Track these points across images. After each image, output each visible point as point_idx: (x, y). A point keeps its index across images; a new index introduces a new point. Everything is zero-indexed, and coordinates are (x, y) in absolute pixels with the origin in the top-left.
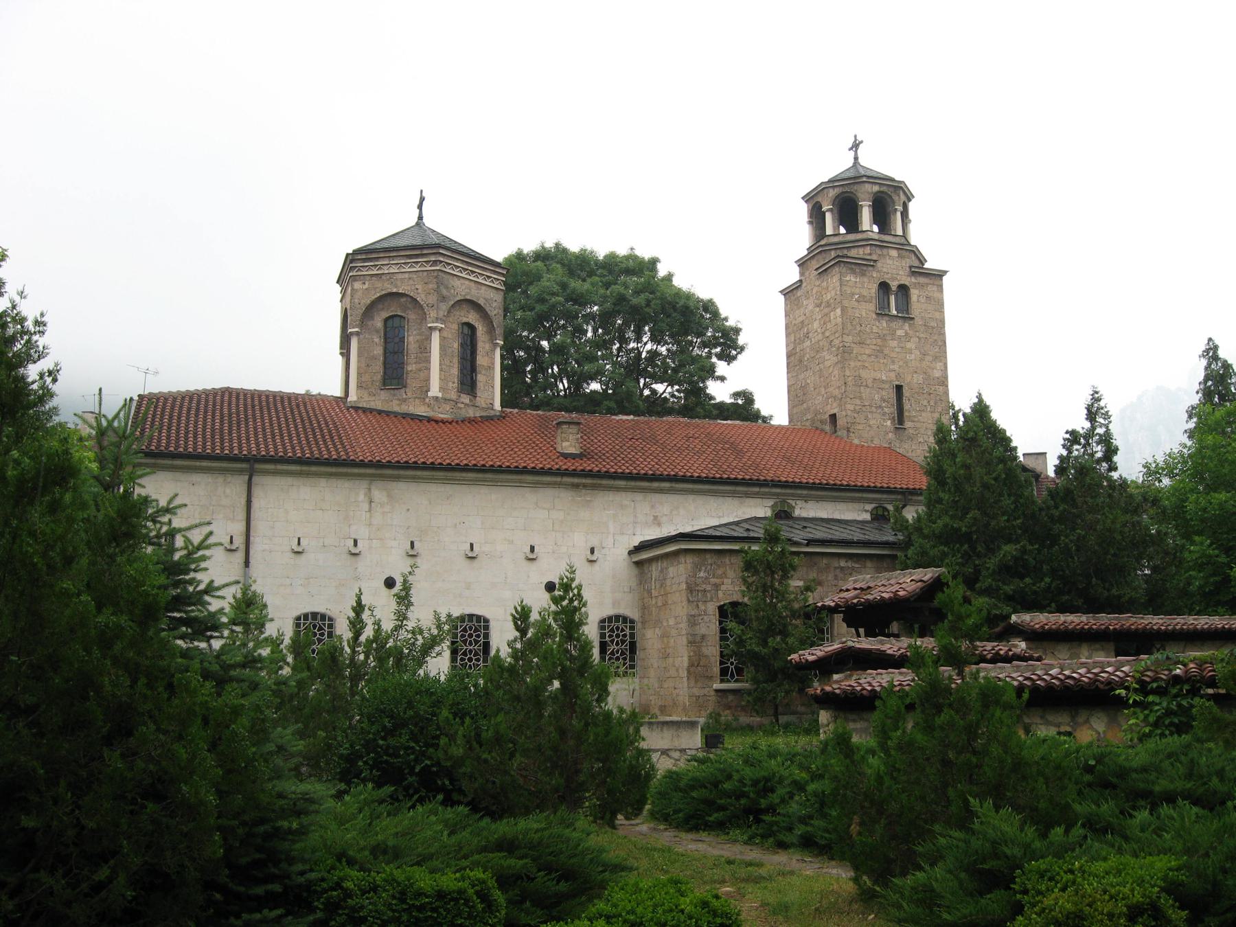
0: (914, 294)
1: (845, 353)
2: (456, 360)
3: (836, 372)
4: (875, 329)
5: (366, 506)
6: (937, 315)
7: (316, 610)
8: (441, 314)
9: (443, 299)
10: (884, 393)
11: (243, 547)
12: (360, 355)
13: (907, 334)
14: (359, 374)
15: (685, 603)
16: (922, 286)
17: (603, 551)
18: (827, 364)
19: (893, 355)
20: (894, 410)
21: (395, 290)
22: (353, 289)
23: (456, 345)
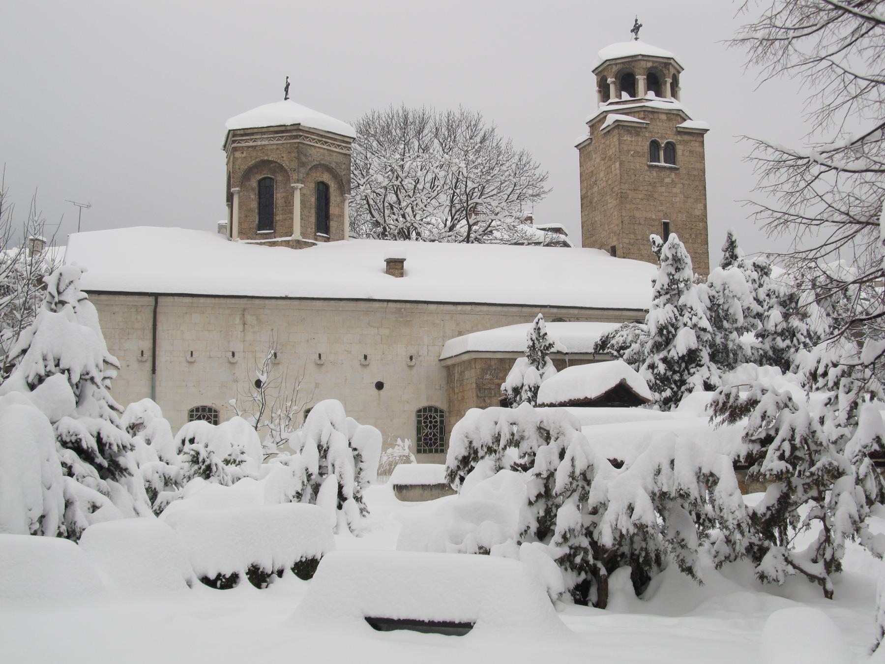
0: (679, 149)
1: (622, 198)
2: (313, 211)
3: (616, 213)
4: (647, 179)
5: (241, 327)
6: (699, 165)
7: (205, 404)
8: (301, 175)
9: (303, 165)
11: (151, 359)
12: (240, 208)
13: (673, 181)
14: (240, 223)
15: (475, 398)
17: (420, 359)
18: (610, 206)
19: (662, 198)
21: (266, 158)
22: (234, 158)
23: (313, 200)
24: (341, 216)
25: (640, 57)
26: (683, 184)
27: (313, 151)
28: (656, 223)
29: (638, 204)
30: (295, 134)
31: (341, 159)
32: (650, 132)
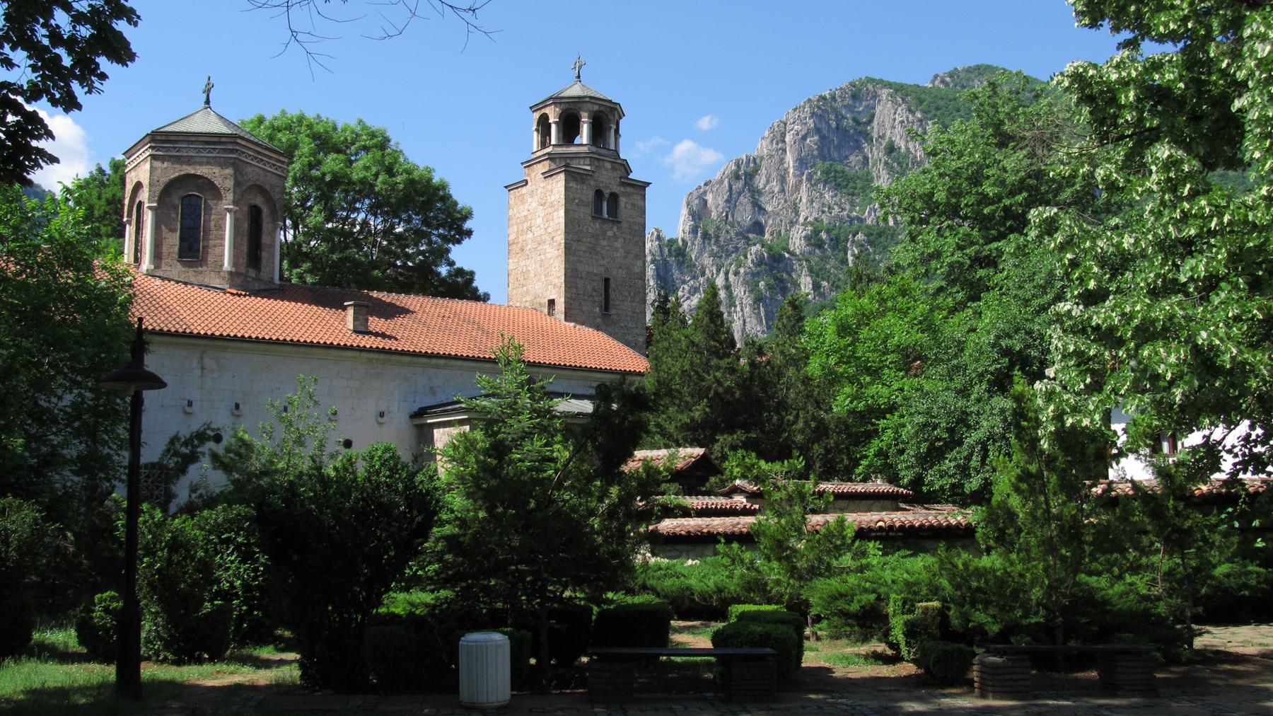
0: (623, 201)
2: (245, 239)
5: (198, 372)
10: (595, 284)
16: (629, 195)
18: (549, 256)
23: (246, 225)
24: (272, 246)
27: (249, 170)
30: (230, 147)
31: (275, 181)
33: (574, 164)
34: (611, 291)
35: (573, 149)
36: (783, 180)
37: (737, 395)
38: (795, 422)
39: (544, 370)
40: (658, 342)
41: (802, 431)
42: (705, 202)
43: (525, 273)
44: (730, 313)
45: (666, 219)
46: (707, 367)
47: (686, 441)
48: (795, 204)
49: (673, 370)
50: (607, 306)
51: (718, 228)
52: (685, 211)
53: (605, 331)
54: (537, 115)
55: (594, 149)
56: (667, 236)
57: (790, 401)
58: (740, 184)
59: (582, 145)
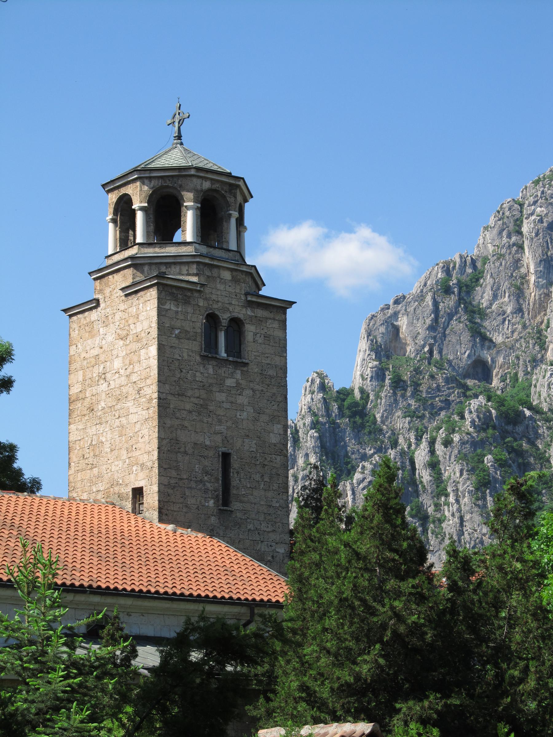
0: (250, 330)
3: (145, 432)
10: (206, 463)
13: (238, 383)
16: (260, 321)
18: (133, 418)
19: (221, 412)
20: (219, 485)
25: (193, 172)
26: (254, 390)
28: (211, 453)
29: (183, 419)
32: (206, 299)
33: (173, 274)
34: (233, 474)
35: (171, 250)
36: (519, 293)
37: (429, 637)
38: (522, 680)
39: (122, 601)
40: (302, 553)
41: (534, 694)
42: (397, 329)
43: (95, 447)
44: (437, 507)
45: (323, 360)
46: (380, 592)
47: (348, 712)
48: (540, 332)
49: (326, 597)
50: (225, 496)
51: (417, 371)
52: (363, 345)
53: (222, 537)
54: (113, 197)
55: (204, 249)
56: (337, 383)
57: (513, 647)
58: (450, 302)
59: (185, 243)
